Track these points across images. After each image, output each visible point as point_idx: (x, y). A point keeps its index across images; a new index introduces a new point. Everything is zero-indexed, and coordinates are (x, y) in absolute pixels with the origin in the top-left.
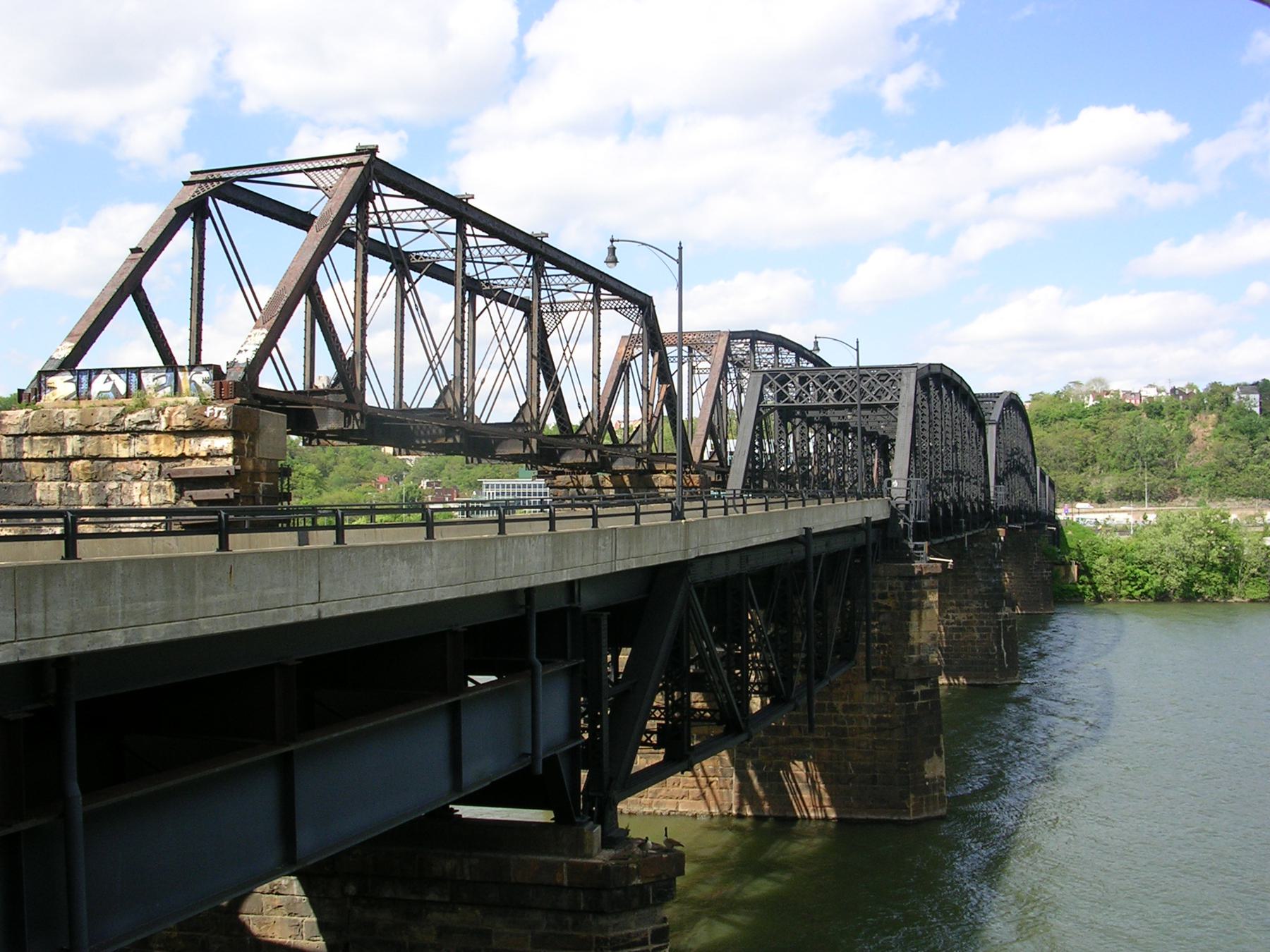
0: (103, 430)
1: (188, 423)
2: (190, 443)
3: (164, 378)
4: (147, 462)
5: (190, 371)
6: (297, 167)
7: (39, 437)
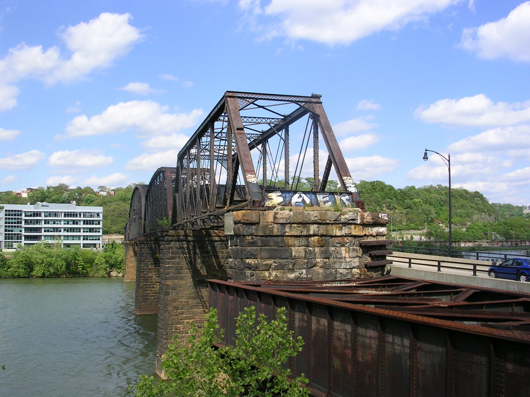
0: (330, 222)
1: (371, 221)
2: (368, 229)
3: (328, 197)
4: (348, 238)
5: (340, 195)
6: (284, 98)
7: (295, 225)
